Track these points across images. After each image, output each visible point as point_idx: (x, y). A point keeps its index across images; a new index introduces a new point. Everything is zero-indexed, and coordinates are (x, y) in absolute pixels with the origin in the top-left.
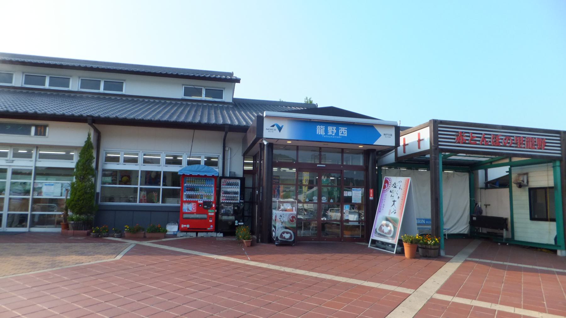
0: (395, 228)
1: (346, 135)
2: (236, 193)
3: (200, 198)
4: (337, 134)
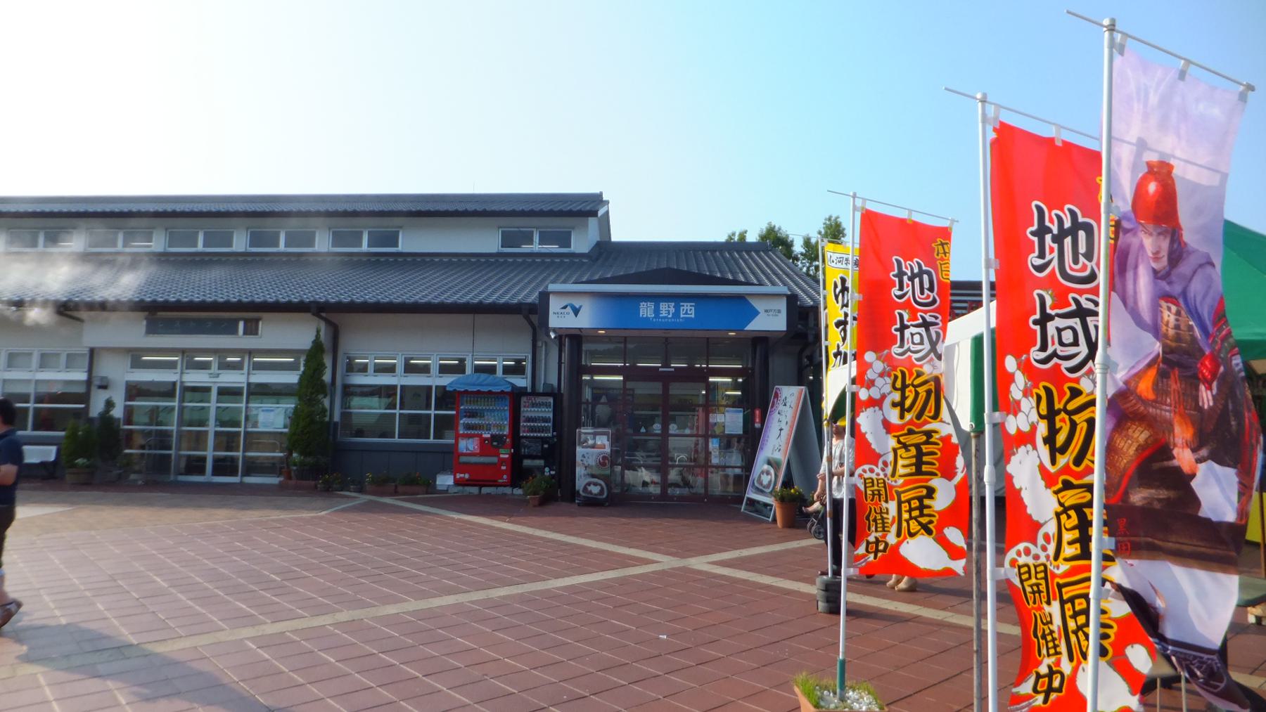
0: (776, 476)
1: (693, 316)
2: (545, 420)
3: (487, 430)
4: (677, 314)
